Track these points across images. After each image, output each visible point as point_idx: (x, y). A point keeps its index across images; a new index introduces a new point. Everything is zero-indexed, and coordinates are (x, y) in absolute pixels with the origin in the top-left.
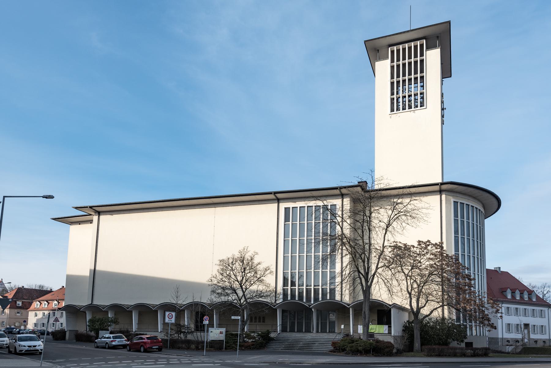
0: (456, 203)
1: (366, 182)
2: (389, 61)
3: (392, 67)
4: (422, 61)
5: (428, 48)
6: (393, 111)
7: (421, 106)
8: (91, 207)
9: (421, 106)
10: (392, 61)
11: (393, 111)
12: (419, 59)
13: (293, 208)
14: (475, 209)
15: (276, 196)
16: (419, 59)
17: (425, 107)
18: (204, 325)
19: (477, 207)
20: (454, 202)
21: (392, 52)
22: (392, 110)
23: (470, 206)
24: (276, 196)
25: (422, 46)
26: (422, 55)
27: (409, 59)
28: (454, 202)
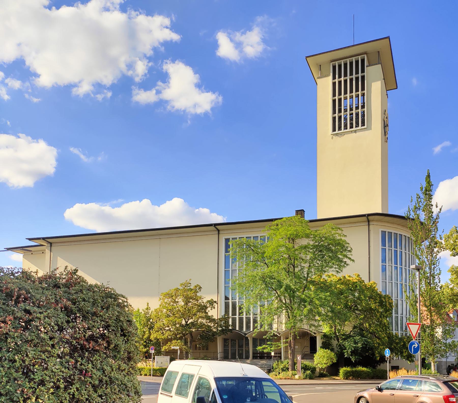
0: (384, 233)
1: (303, 210)
2: (331, 77)
3: (334, 84)
4: (363, 77)
5: (370, 65)
6: (347, 129)
7: (356, 127)
8: (44, 239)
9: (356, 127)
10: (334, 78)
11: (347, 129)
12: (360, 75)
13: (254, 237)
14: (407, 238)
15: (216, 228)
16: (360, 75)
17: (365, 127)
18: (226, 384)
19: (406, 235)
20: (382, 231)
21: (334, 67)
22: (334, 130)
23: (403, 236)
24: (216, 228)
25: (363, 61)
26: (363, 71)
27: (356, 74)
28: (382, 231)
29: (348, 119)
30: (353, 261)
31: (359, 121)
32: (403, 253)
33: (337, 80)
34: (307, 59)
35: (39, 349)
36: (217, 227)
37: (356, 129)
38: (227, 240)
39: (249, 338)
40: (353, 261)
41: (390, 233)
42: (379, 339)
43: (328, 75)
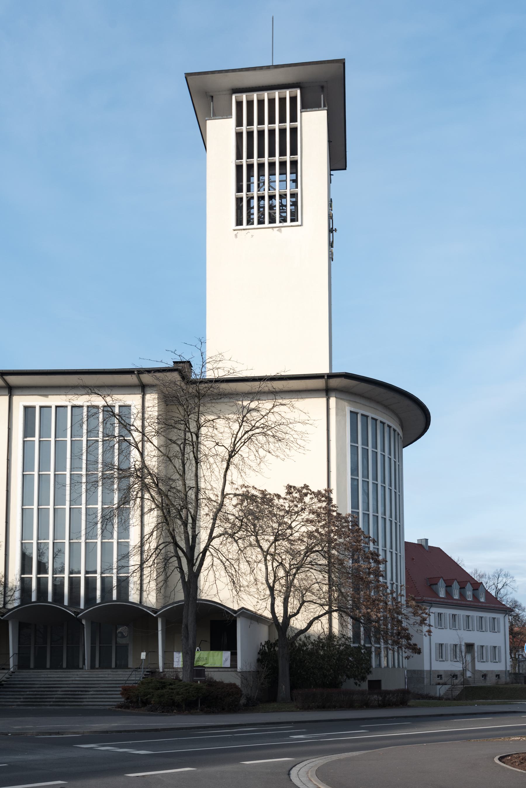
2: (233, 121)
3: (239, 135)
10: (239, 123)
17: (299, 223)
21: (239, 104)
22: (239, 222)
23: (378, 422)
25: (293, 100)
26: (294, 119)
29: (264, 204)
30: (234, 230)
31: (289, 211)
33: (244, 129)
34: (188, 78)
35: (175, 691)
37: (281, 225)
38: (28, 410)
39: (84, 622)
40: (234, 230)
42: (341, 592)
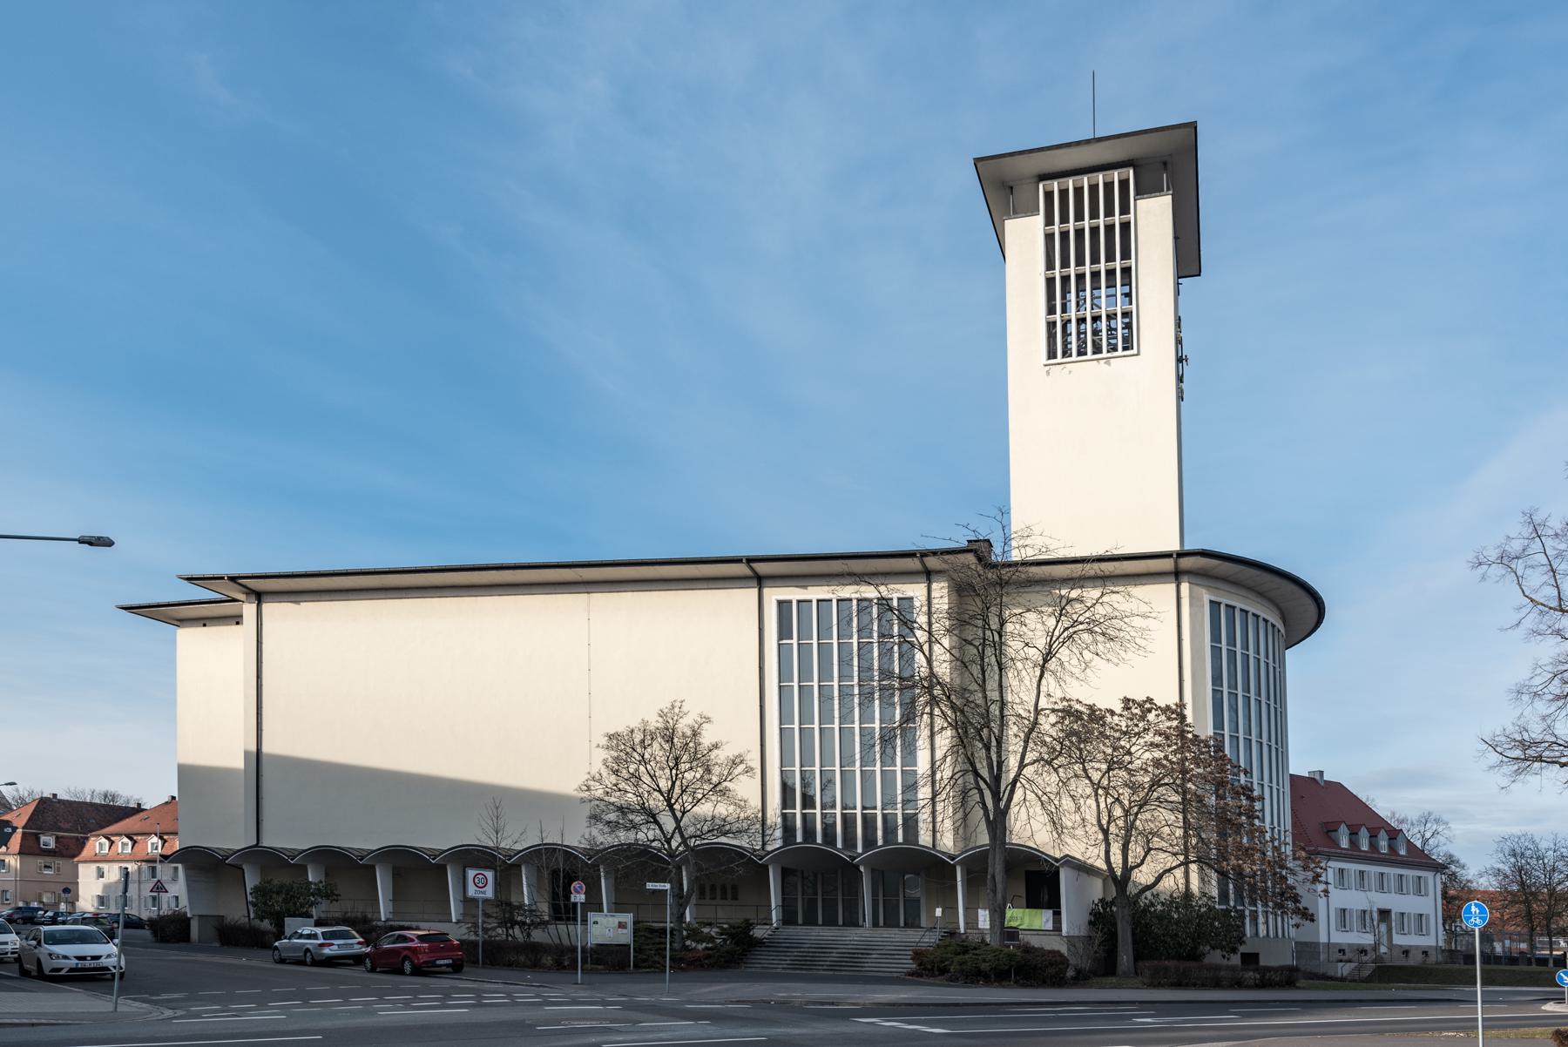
0: (1215, 605)
2: (1040, 219)
3: (1049, 238)
8: (233, 579)
9: (1125, 349)
10: (1049, 221)
12: (1117, 219)
15: (752, 569)
17: (1135, 351)
22: (1052, 354)
24: (752, 569)
25: (1124, 184)
26: (1125, 209)
27: (1076, 220)
31: (1121, 336)
32: (1263, 665)
36: (754, 565)
38: (783, 606)
41: (1230, 608)
43: (1035, 211)
